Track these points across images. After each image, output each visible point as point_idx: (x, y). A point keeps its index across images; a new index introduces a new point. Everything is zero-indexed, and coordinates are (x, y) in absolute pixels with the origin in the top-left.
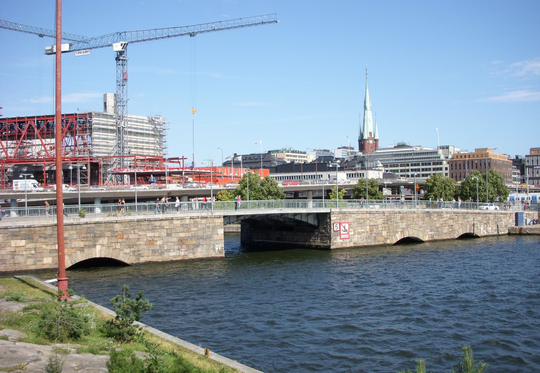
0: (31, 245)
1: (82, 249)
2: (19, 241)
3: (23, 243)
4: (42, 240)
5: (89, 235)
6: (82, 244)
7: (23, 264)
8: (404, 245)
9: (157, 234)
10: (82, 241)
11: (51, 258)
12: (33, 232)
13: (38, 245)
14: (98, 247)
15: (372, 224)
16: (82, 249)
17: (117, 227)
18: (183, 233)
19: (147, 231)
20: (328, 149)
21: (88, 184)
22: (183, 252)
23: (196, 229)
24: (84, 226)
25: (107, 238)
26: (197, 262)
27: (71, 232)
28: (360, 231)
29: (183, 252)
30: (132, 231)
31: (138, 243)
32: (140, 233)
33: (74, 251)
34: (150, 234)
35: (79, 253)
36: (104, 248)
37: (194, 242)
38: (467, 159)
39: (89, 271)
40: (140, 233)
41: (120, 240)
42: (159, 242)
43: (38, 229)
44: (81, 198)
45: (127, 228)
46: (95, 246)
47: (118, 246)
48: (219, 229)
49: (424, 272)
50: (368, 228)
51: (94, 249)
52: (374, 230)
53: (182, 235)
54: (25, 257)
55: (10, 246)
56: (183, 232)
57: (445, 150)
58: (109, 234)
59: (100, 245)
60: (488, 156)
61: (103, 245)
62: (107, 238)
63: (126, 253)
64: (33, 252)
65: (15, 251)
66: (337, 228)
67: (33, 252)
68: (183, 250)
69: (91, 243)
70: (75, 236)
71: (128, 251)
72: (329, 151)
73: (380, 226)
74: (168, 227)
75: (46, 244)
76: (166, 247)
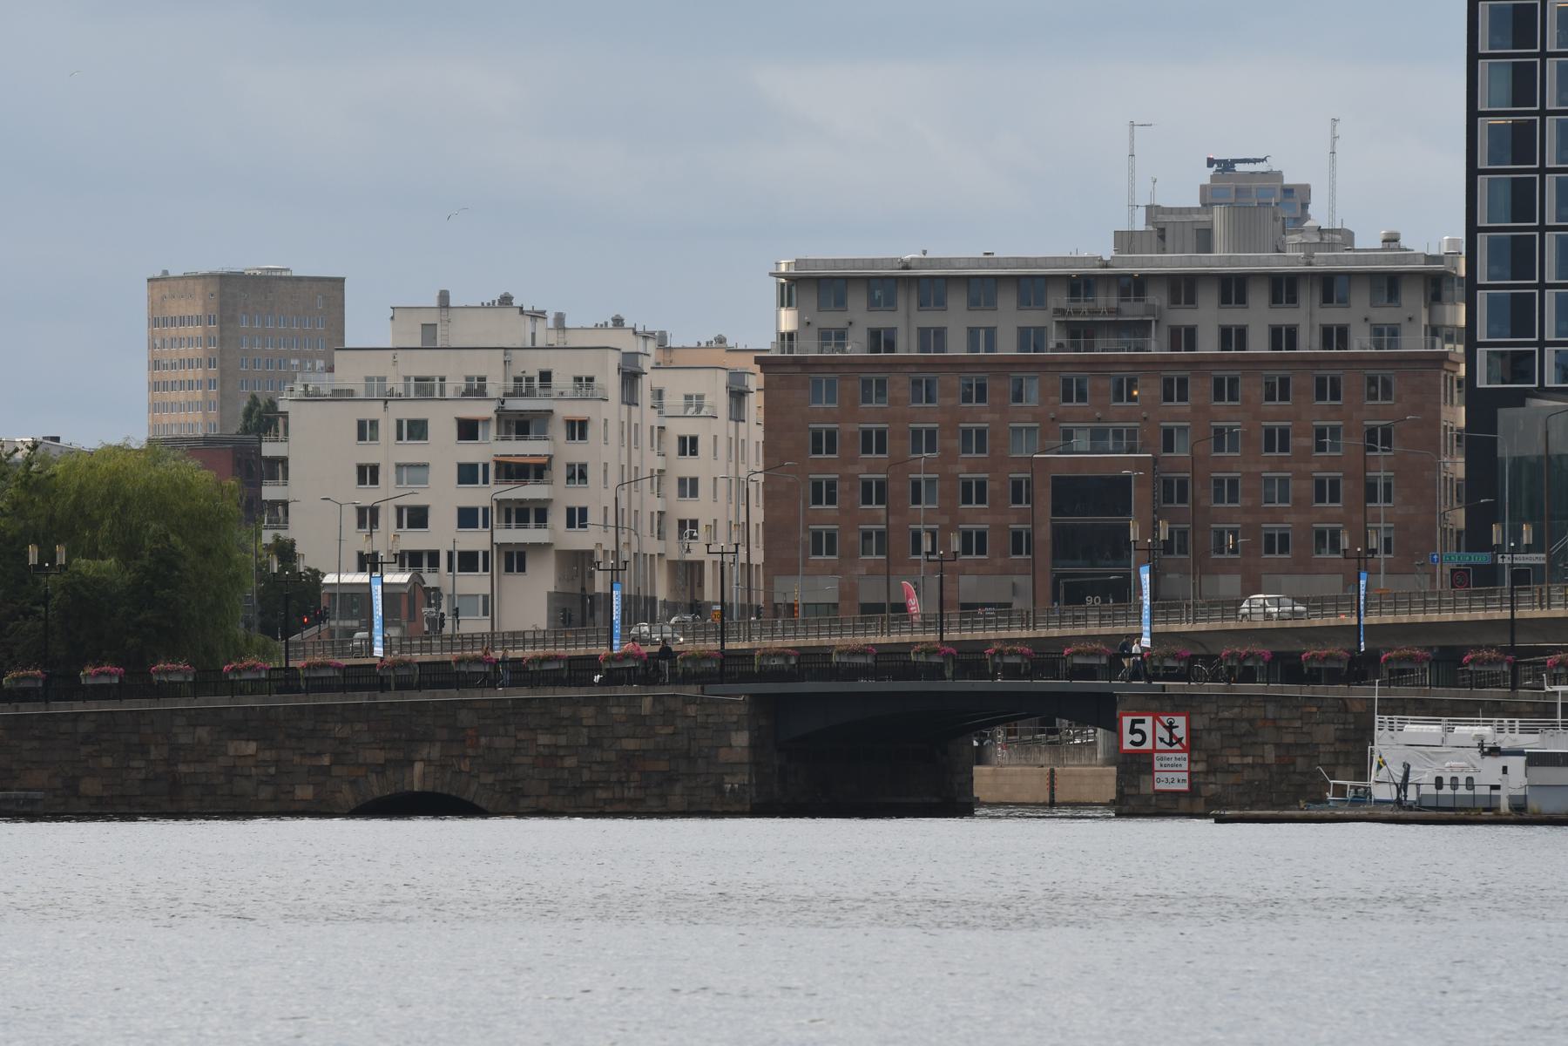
0: (268, 755)
1: (380, 769)
2: (243, 742)
3: (251, 747)
5: (397, 735)
6: (380, 756)
8: (723, 818)
9: (562, 740)
10: (381, 749)
11: (311, 787)
14: (418, 767)
15: (1289, 739)
16: (380, 769)
17: (465, 717)
18: (632, 741)
19: (539, 731)
20: (425, 461)
22: (632, 790)
23: (669, 730)
25: (438, 745)
27: (358, 727)
28: (1235, 760)
29: (632, 790)
30: (501, 730)
31: (516, 760)
32: (521, 735)
34: (543, 739)
35: (373, 778)
36: (432, 768)
37: (662, 766)
38: (1386, 337)
39: (391, 820)
40: (521, 735)
41: (470, 752)
42: (570, 762)
45: (488, 722)
46: (411, 763)
47: (465, 766)
48: (733, 734)
49: (467, 907)
50: (1270, 755)
52: (1300, 761)
53: (630, 744)
55: (225, 754)
56: (634, 737)
59: (422, 760)
61: (430, 761)
62: (438, 745)
63: (485, 785)
65: (234, 766)
66: (1138, 737)
67: (272, 770)
68: (632, 785)
69: (402, 755)
71: (490, 779)
73: (1322, 749)
74: (591, 722)
76: (586, 775)
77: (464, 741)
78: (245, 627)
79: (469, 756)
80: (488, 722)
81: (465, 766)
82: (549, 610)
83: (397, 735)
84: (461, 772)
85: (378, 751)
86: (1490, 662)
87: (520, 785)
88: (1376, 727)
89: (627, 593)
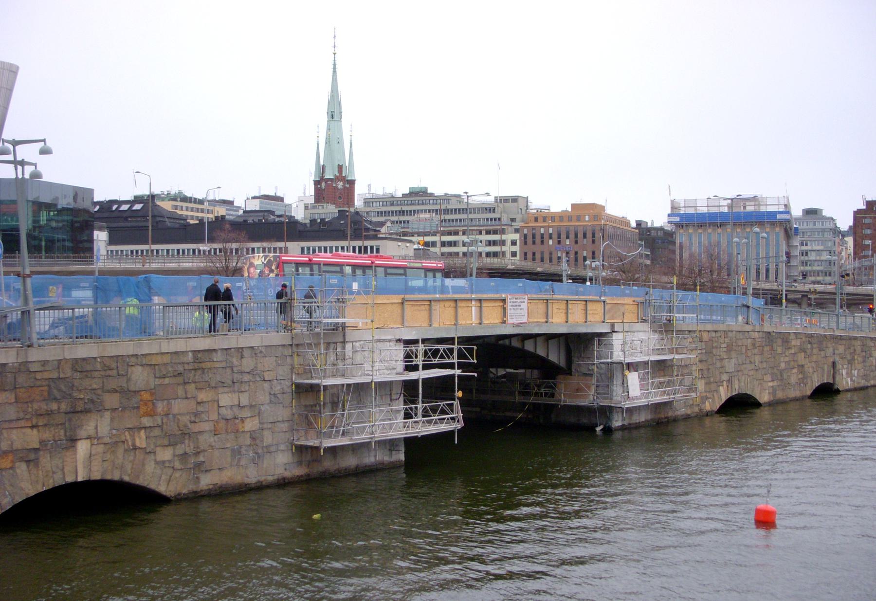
5: (54, 406)
9: (245, 400)
10: (32, 427)
14: (83, 447)
17: (140, 377)
31: (195, 428)
35: (22, 468)
36: (101, 448)
40: (202, 396)
41: (147, 421)
46: (73, 441)
58: (112, 400)
59: (89, 438)
62: (107, 415)
63: (164, 462)
71: (165, 455)
77: (138, 408)
78: (193, 286)
79: (145, 428)
80: (167, 381)
81: (141, 440)
82: (354, 190)
83: (54, 406)
84: (135, 448)
85: (29, 431)
86: (648, 478)
87: (202, 459)
88: (305, 244)
89: (20, 176)
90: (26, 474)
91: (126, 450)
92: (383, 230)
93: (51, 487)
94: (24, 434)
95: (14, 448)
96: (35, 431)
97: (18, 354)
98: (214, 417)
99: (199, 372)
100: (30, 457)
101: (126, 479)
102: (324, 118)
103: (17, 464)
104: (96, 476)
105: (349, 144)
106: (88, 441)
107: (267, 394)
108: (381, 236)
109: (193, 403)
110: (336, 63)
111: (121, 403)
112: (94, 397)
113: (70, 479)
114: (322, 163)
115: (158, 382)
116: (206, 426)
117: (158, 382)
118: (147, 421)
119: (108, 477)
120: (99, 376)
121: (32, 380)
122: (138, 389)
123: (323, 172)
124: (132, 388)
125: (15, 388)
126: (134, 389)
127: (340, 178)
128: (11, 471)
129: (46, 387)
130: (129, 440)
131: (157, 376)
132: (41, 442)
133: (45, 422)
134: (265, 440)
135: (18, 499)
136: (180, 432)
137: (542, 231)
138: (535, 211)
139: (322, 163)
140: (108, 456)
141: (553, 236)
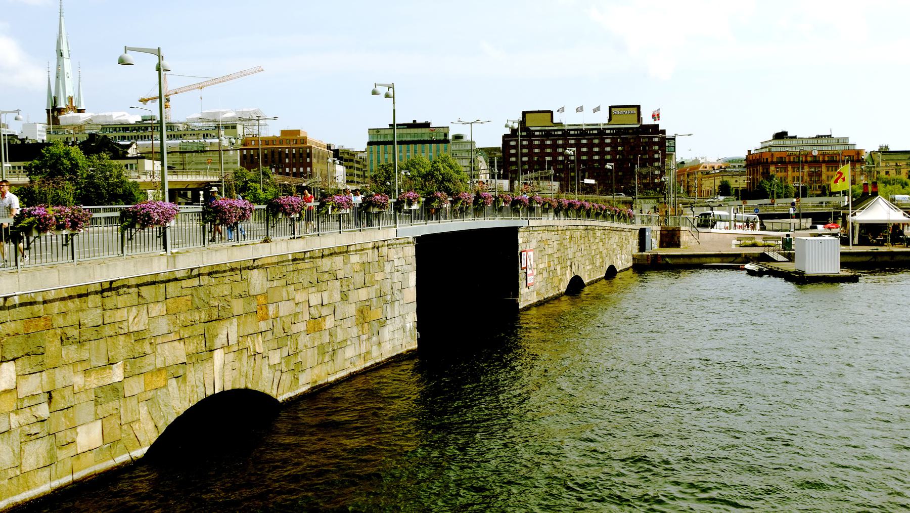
0: (33, 385)
4: (71, 352)
7: (11, 473)
12: (42, 323)
13: (61, 377)
16: (178, 373)
21: (740, 189)
24: (185, 283)
26: (690, 499)
33: (159, 381)
41: (263, 326)
43: (56, 307)
44: (169, 190)
51: (207, 365)
54: (16, 437)
57: (230, 130)
58: (238, 306)
60: (306, 143)
64: (43, 411)
70: (163, 325)
72: (427, 125)
75: (85, 366)
85: (176, 343)
90: (176, 391)
91: (249, 356)
92: (130, 151)
93: (195, 403)
94: (174, 348)
95: (167, 365)
96: (182, 342)
97: (168, 262)
98: (307, 317)
99: (296, 273)
100: (178, 373)
101: (250, 386)
102: (55, 55)
103: (169, 381)
104: (228, 387)
105: (47, 79)
106: (222, 350)
107: (339, 292)
108: (129, 156)
109: (291, 303)
110: (63, 11)
111: (244, 309)
112: (225, 304)
113: (210, 392)
114: (53, 95)
115: (269, 284)
116: (301, 327)
117: (269, 284)
118: (263, 326)
119: (237, 387)
120: (229, 282)
121: (180, 289)
122: (255, 294)
123: (55, 102)
124: (252, 293)
125: (166, 299)
126: (253, 294)
127: (70, 107)
128: (165, 390)
129: (190, 296)
130: (251, 346)
131: (269, 279)
132: (189, 356)
133: (190, 334)
134: (338, 337)
135: (171, 420)
136: (285, 334)
137: (287, 151)
138: (251, 136)
139: (53, 95)
140: (237, 365)
141: (296, 156)
